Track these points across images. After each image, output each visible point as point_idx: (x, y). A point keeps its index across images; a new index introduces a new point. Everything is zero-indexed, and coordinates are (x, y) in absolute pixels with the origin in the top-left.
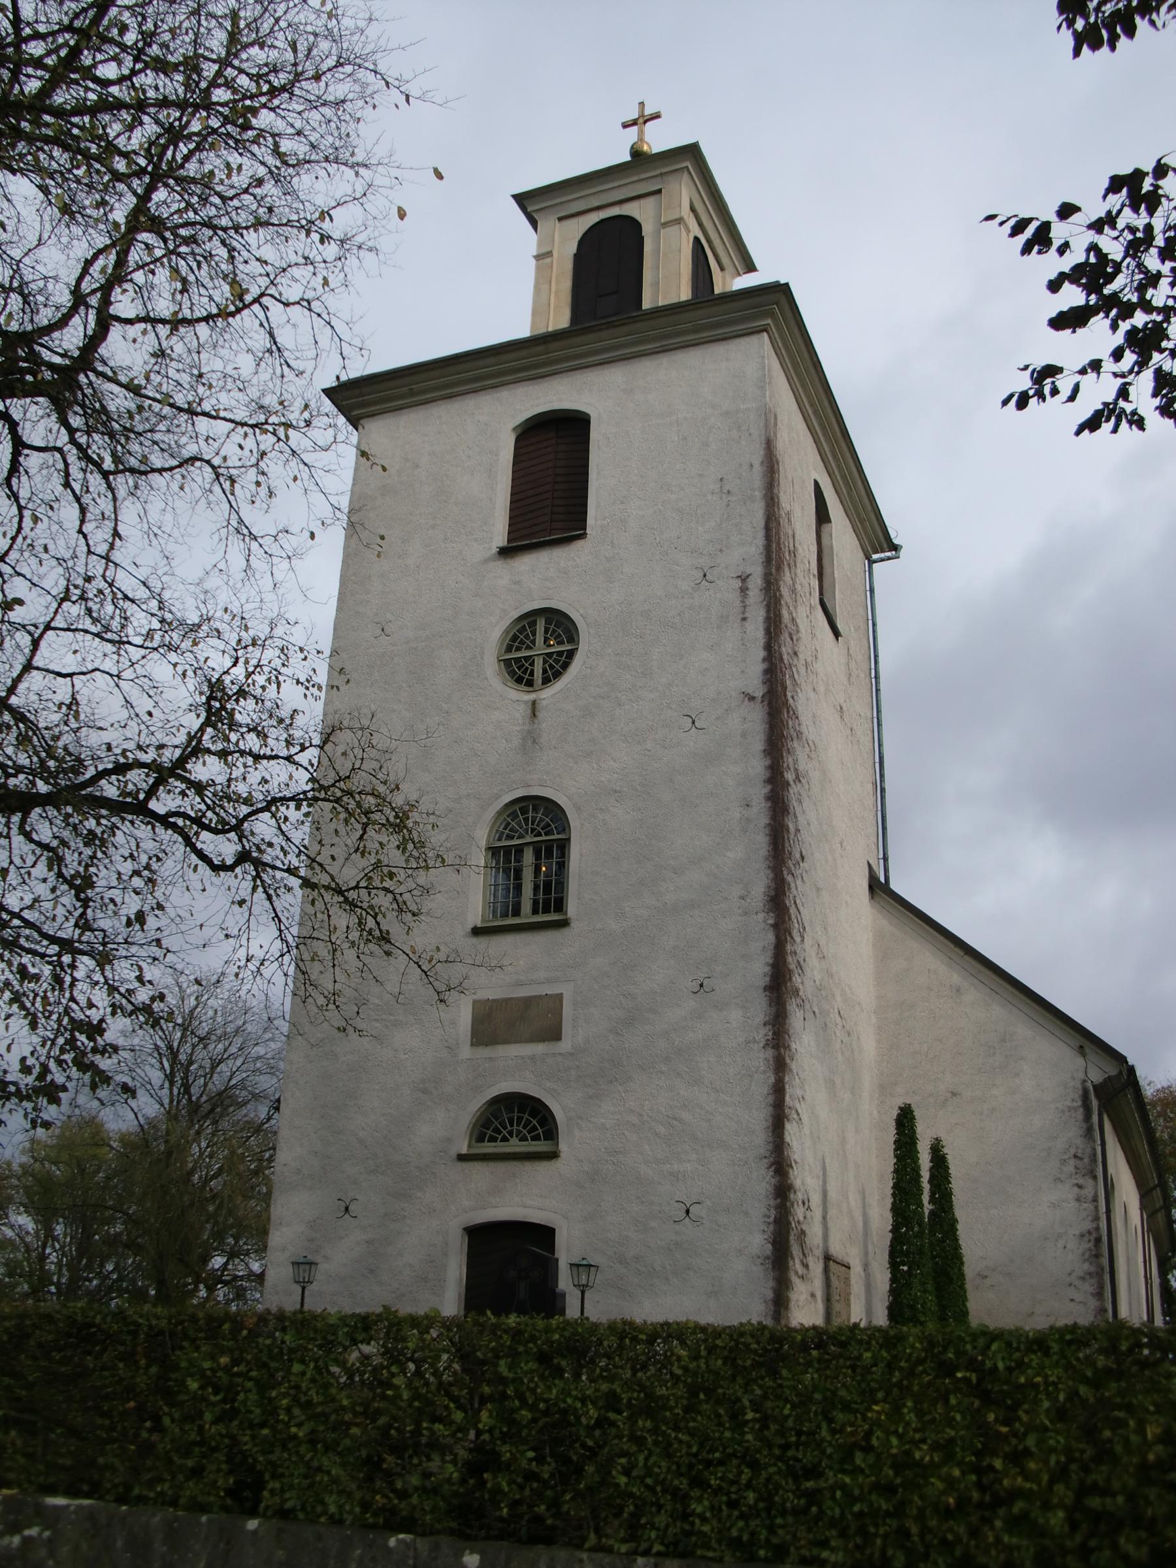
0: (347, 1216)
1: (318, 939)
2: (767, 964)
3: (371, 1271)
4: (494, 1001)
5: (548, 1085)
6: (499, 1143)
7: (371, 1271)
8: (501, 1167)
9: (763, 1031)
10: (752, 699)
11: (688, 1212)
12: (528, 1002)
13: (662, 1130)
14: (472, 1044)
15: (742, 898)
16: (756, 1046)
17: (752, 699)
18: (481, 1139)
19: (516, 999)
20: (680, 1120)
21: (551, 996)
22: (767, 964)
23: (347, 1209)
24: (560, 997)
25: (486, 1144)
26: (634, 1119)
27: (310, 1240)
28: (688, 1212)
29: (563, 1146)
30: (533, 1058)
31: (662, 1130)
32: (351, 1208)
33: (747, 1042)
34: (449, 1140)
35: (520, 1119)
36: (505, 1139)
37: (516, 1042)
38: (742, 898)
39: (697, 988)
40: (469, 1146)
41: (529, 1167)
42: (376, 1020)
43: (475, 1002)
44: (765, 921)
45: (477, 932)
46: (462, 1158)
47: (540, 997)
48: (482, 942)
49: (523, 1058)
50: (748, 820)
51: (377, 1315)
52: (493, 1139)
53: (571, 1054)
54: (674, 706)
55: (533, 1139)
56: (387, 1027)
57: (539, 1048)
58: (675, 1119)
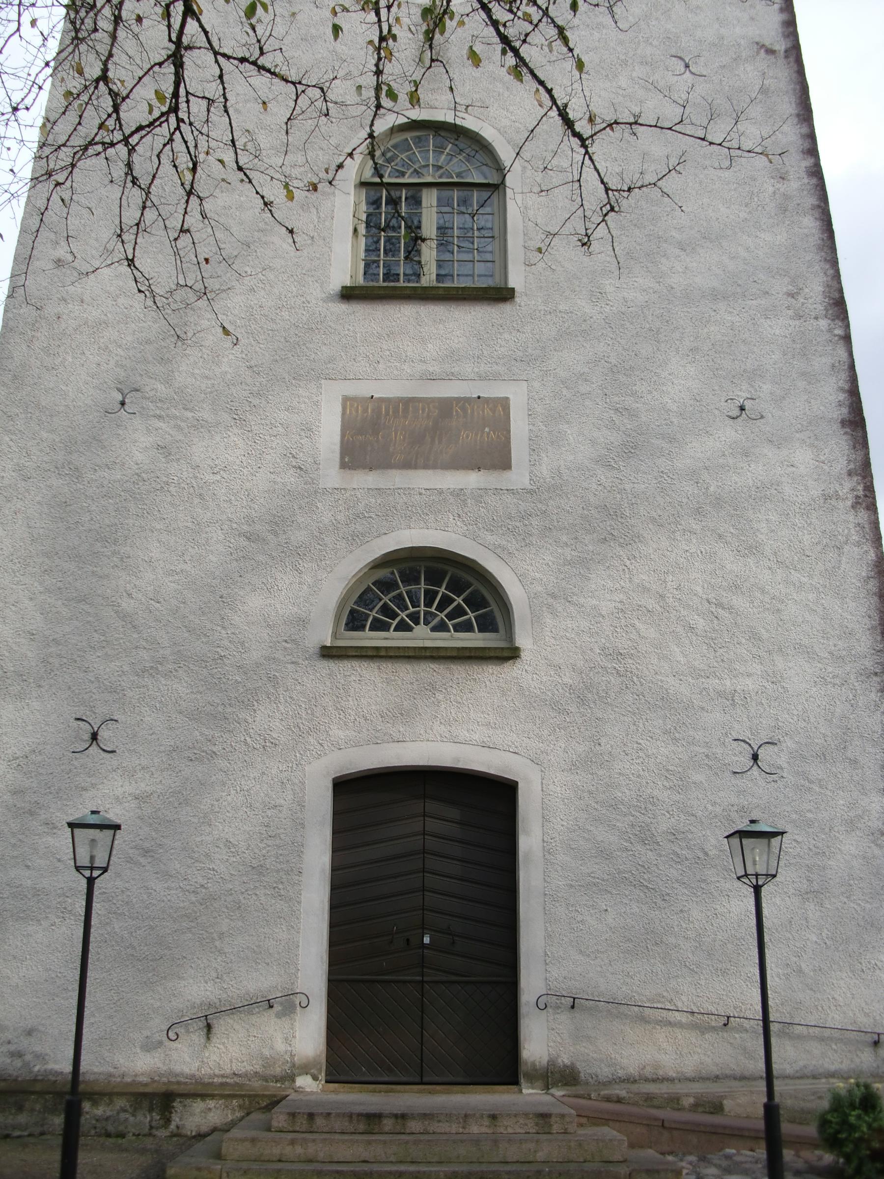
0: (94, 749)
1: (131, 90)
2: (842, 389)
3: (146, 852)
4: (381, 400)
5: (490, 538)
6: (392, 633)
7: (146, 852)
8: (427, 671)
9: (848, 484)
10: (770, 52)
11: (755, 757)
12: (446, 406)
13: (700, 623)
14: (343, 466)
15: (792, 295)
16: (841, 505)
17: (770, 52)
18: (355, 622)
19: (432, 400)
20: (730, 609)
21: (488, 400)
22: (842, 389)
23: (94, 736)
24: (504, 403)
25: (367, 633)
26: (651, 603)
27: (17, 792)
28: (755, 757)
29: (522, 640)
30: (459, 494)
31: (700, 623)
32: (103, 734)
33: (826, 498)
34: (303, 622)
35: (430, 597)
36: (403, 627)
37: (426, 467)
38: (792, 295)
39: (736, 412)
40: (335, 635)
41: (459, 671)
42: (159, 417)
43: (346, 400)
44: (830, 330)
45: (348, 294)
46: (328, 653)
47: (467, 400)
48: (360, 311)
49: (441, 492)
50: (786, 197)
51: (557, 1086)
52: (378, 626)
53: (531, 492)
54: (655, 43)
55: (458, 628)
56: (179, 428)
57: (471, 480)
58: (720, 605)
